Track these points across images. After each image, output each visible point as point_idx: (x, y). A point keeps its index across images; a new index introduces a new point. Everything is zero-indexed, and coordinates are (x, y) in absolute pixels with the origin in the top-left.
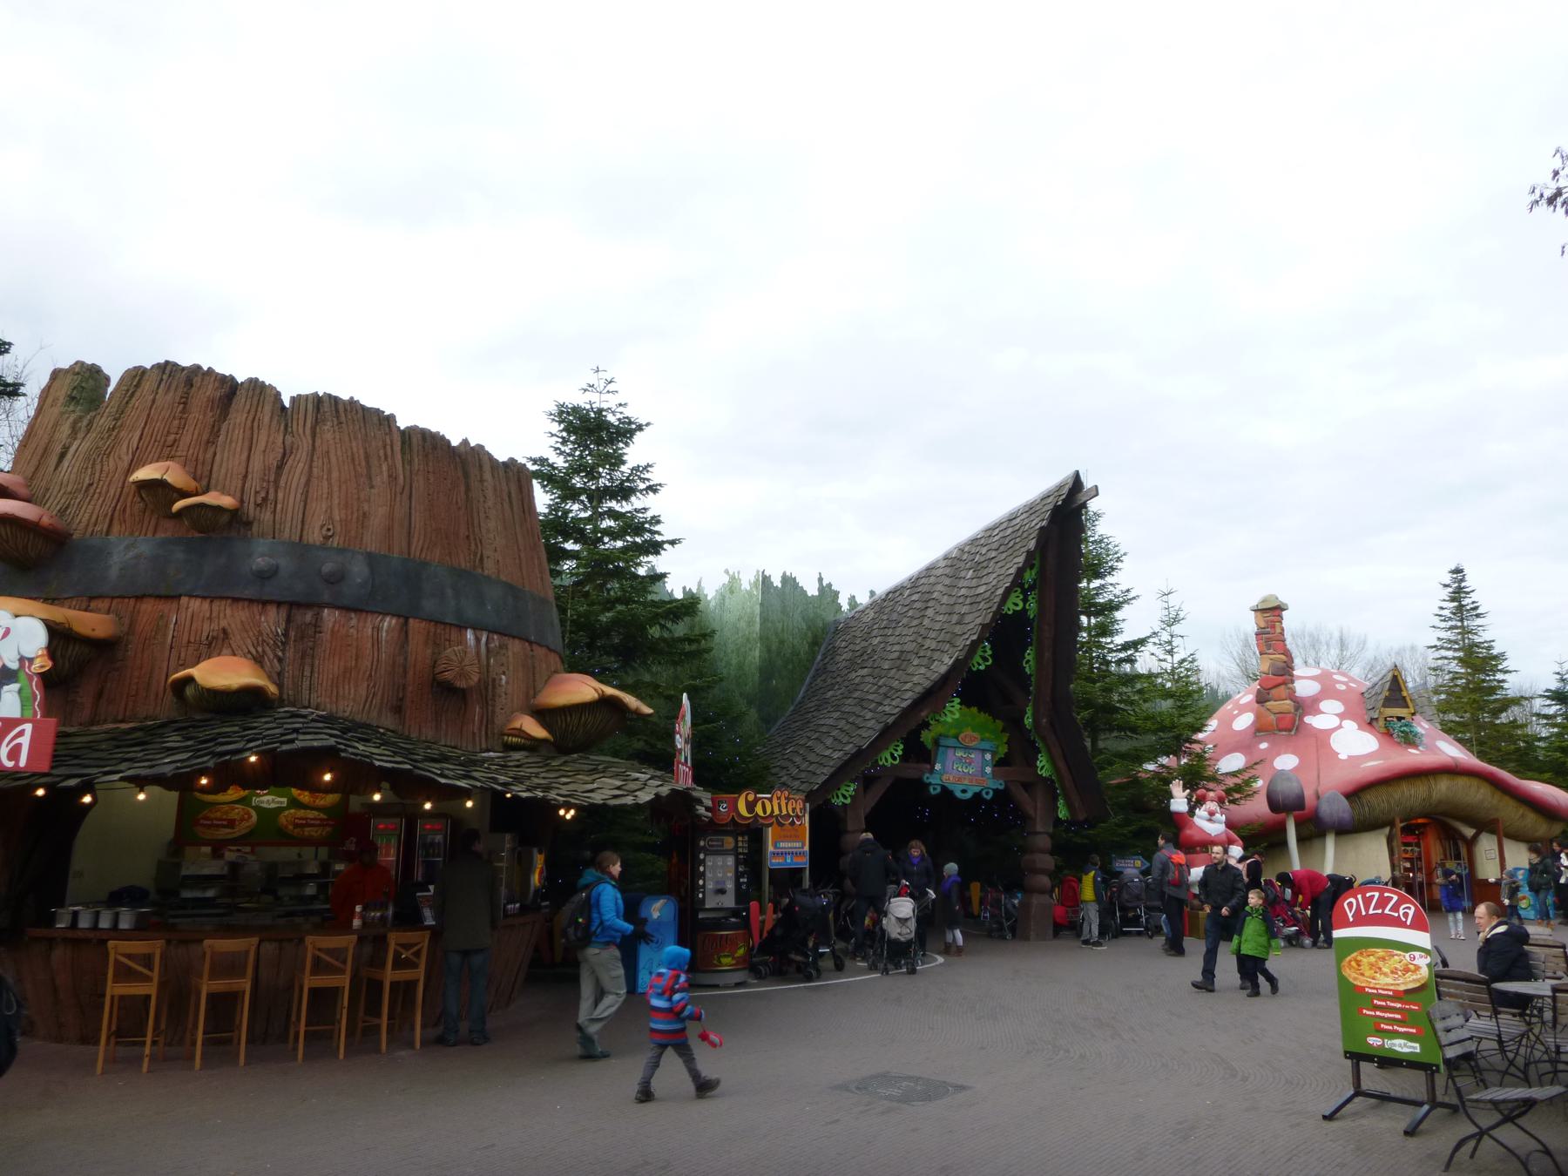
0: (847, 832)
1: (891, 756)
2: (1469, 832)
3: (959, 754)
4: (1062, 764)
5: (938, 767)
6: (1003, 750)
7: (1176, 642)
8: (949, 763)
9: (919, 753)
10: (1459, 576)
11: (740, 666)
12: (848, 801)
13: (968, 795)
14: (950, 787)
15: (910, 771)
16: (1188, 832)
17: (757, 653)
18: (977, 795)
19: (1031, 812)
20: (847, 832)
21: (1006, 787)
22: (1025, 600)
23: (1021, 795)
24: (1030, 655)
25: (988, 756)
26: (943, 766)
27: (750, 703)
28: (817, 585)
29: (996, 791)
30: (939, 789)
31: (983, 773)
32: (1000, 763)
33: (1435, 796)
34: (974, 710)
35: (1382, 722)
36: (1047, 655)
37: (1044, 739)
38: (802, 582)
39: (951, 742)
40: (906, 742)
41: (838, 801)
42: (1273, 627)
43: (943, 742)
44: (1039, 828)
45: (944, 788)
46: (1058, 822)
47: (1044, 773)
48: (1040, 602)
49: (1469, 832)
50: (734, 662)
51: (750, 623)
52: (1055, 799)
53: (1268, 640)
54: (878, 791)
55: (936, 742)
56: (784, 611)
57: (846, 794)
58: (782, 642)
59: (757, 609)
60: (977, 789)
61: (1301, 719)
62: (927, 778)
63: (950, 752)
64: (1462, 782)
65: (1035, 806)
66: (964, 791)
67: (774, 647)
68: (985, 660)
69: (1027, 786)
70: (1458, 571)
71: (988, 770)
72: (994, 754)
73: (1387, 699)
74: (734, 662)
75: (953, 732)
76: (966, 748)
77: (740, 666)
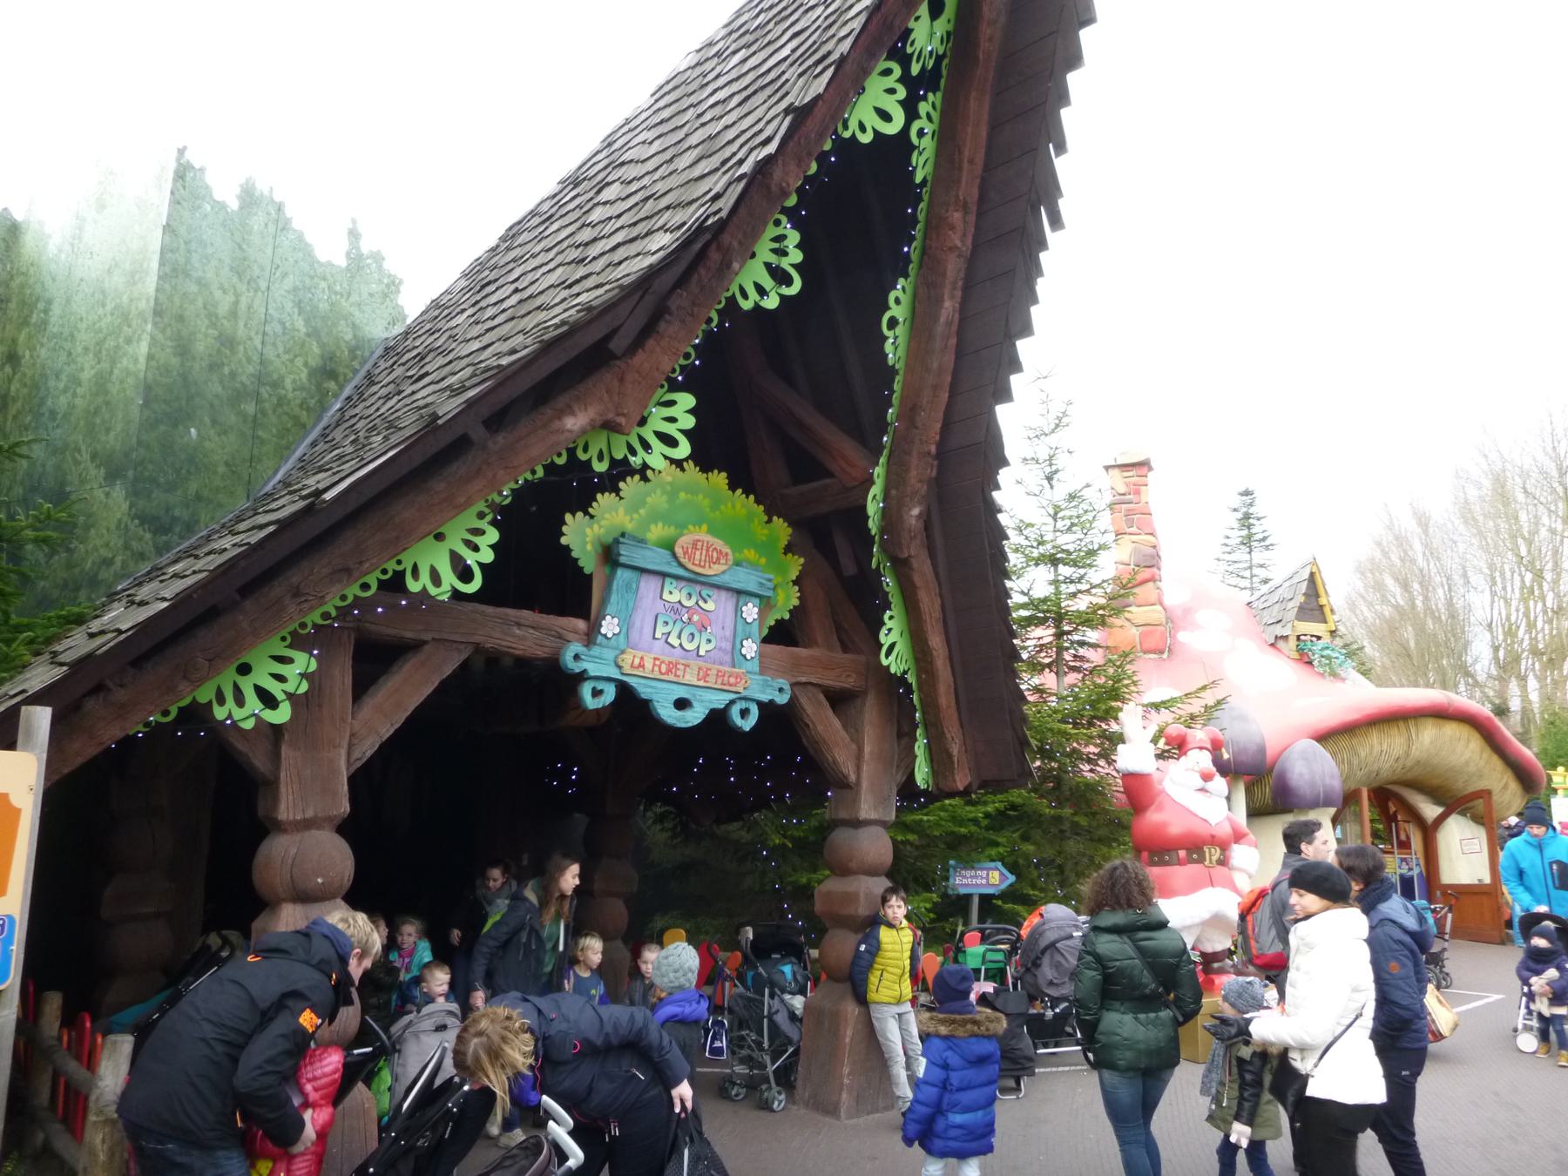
0: (278, 827)
1: (449, 557)
2: (1431, 811)
3: (675, 594)
4: (936, 641)
5: (609, 626)
6: (787, 600)
7: (1060, 462)
8: (642, 620)
9: (541, 575)
10: (1247, 499)
11: (101, 384)
12: (282, 715)
13: (694, 717)
14: (644, 690)
15: (522, 633)
16: (1153, 817)
17: (143, 349)
18: (717, 718)
19: (849, 770)
20: (278, 827)
21: (793, 700)
22: (911, 114)
23: (824, 722)
24: (899, 302)
25: (751, 611)
26: (627, 625)
27: (113, 475)
28: (344, 245)
29: (766, 708)
30: (610, 694)
31: (736, 656)
32: (779, 635)
33: (1416, 752)
34: (720, 479)
35: (1293, 642)
36: (949, 307)
37: (901, 567)
38: (301, 218)
39: (655, 558)
40: (506, 519)
41: (246, 714)
42: (1138, 493)
43: (626, 554)
44: (866, 810)
45: (624, 690)
46: (908, 791)
47: (896, 662)
48: (947, 137)
49: (1431, 811)
50: (87, 375)
51: (133, 278)
52: (905, 736)
53: (1129, 513)
54: (405, 692)
55: (609, 555)
56: (241, 268)
57: (265, 687)
58: (228, 342)
59: (156, 240)
60: (719, 700)
61: (1173, 637)
62: (573, 656)
63: (649, 586)
64: (1451, 729)
65: (858, 753)
66: (682, 704)
67: (200, 346)
68: (781, 277)
69: (839, 700)
70: (1247, 493)
71: (750, 648)
72: (766, 604)
73: (1301, 608)
74: (87, 375)
75: (656, 532)
76: (694, 580)
77: (101, 384)
